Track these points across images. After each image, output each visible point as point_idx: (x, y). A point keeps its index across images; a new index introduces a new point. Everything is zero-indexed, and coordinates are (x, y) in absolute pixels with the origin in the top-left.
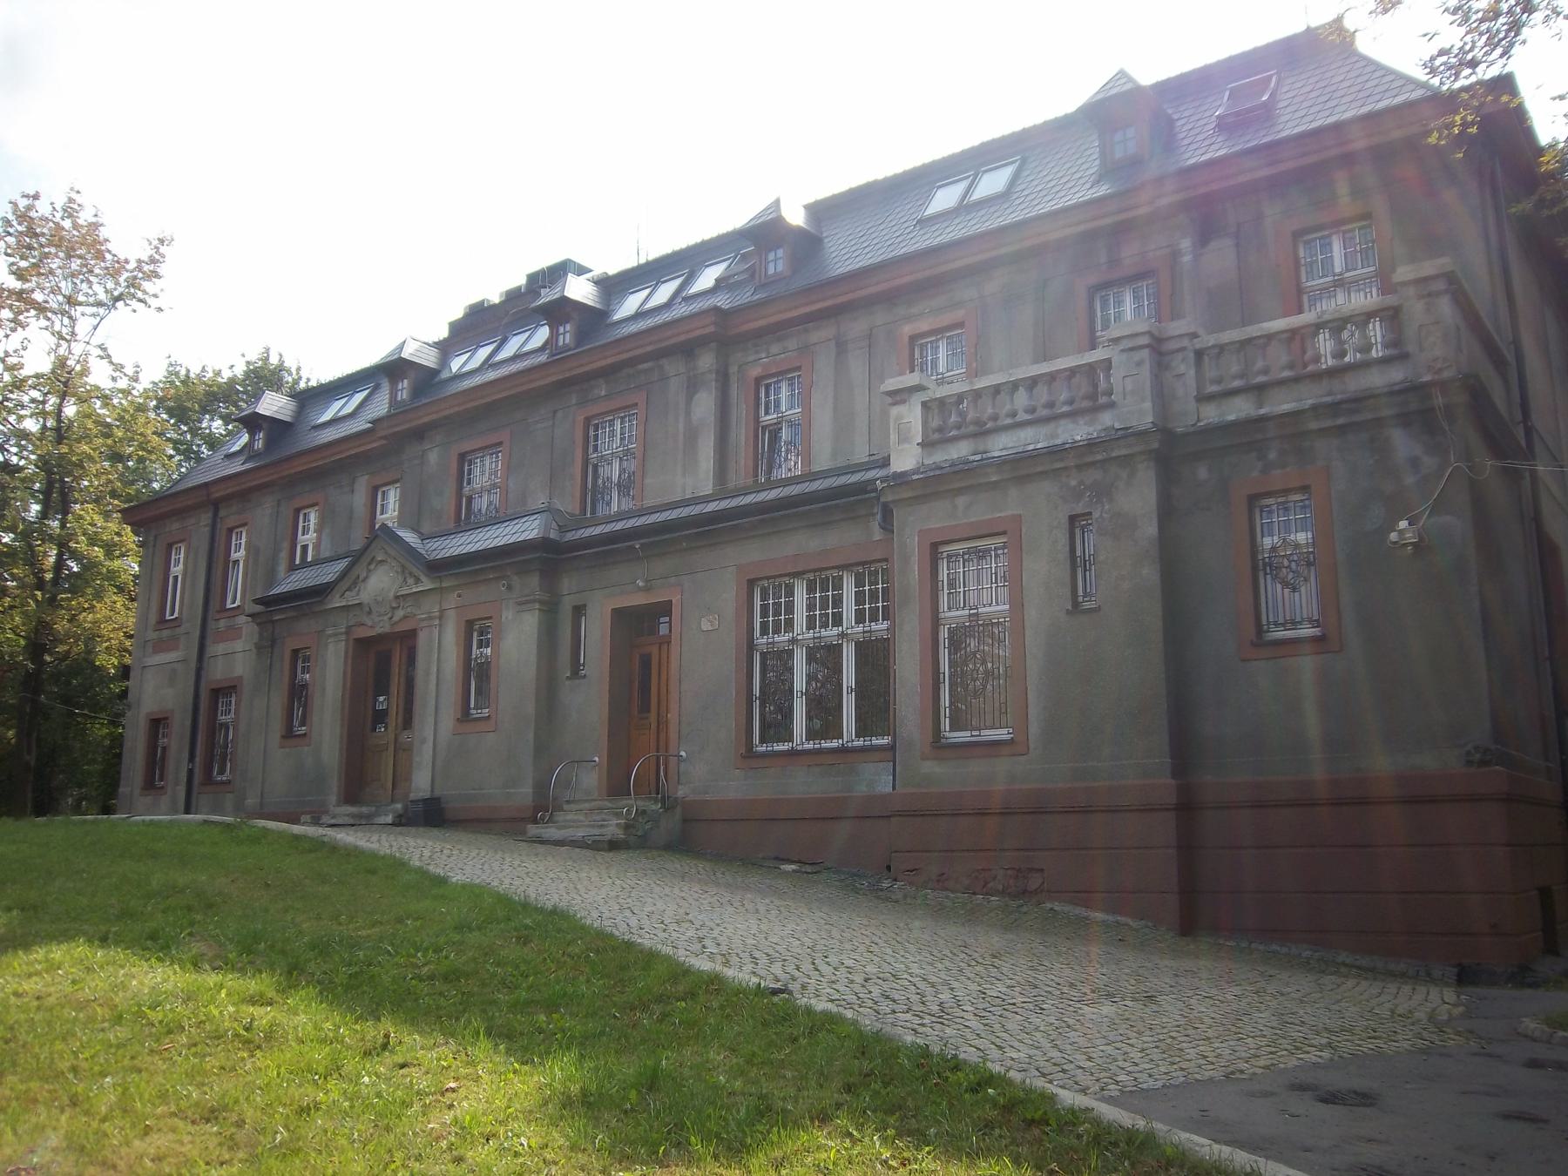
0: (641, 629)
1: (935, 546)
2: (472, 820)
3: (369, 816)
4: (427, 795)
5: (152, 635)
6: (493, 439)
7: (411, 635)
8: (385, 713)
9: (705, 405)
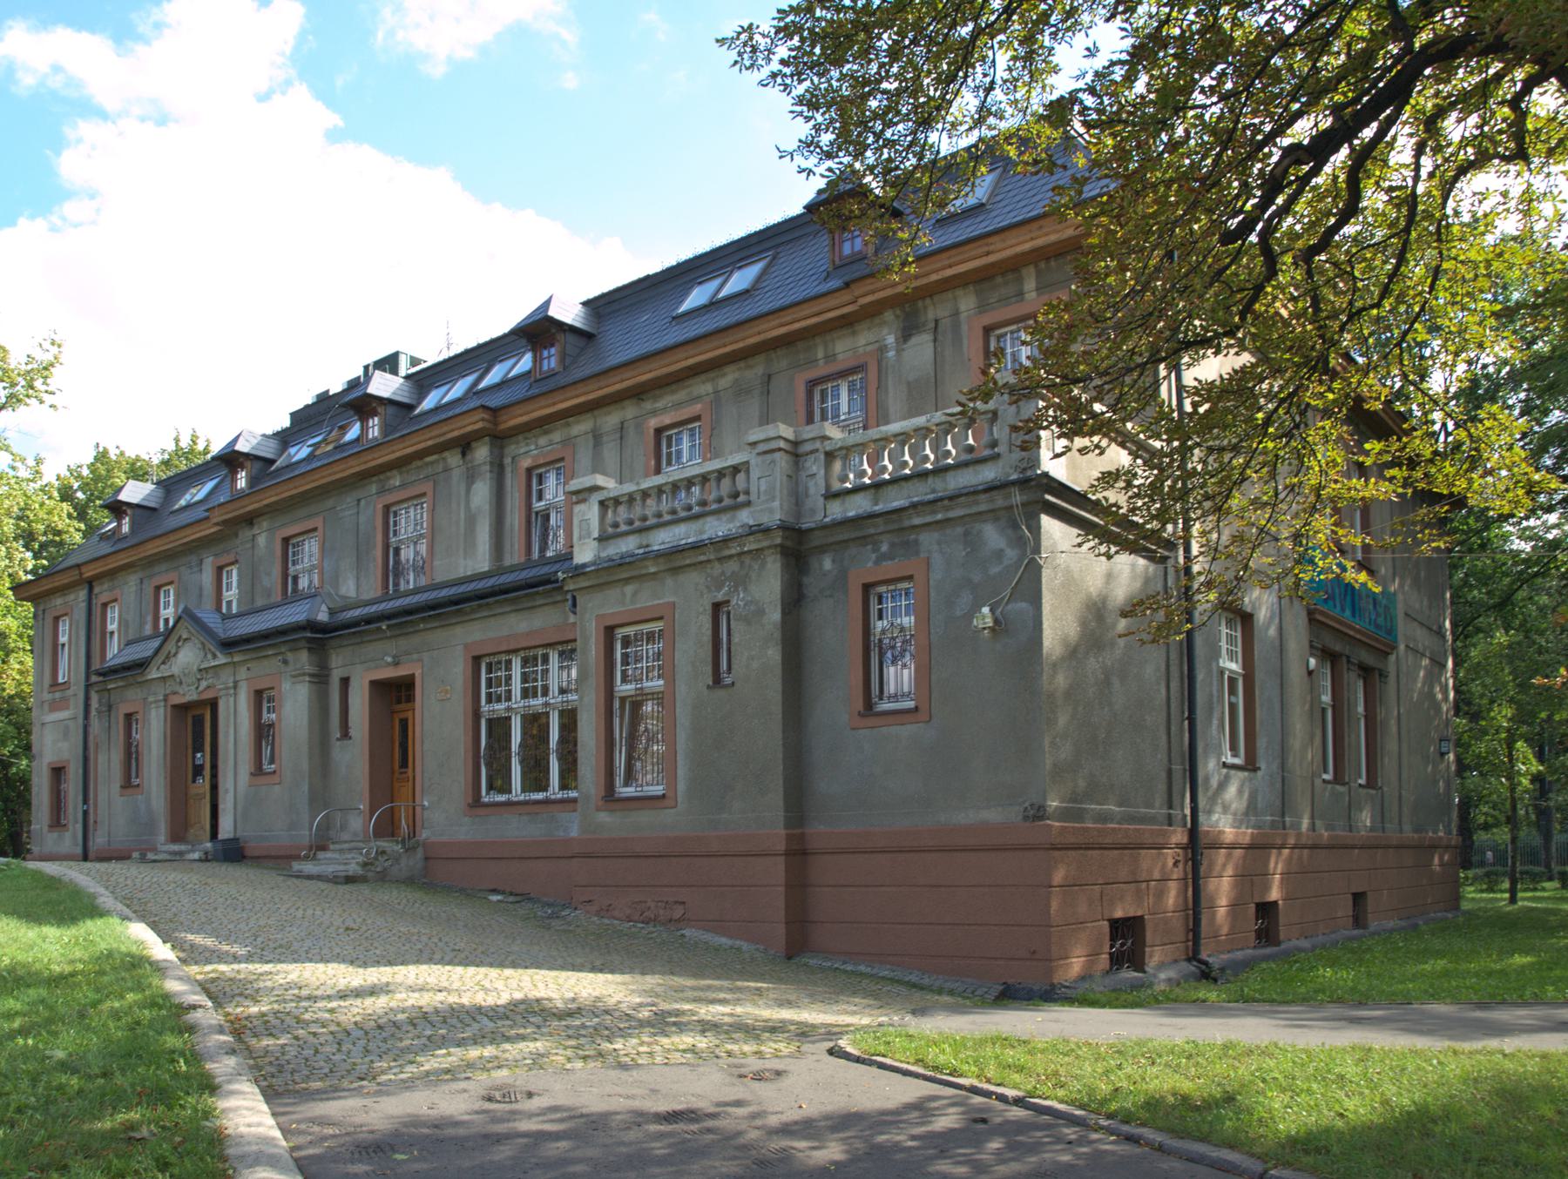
0: (395, 694)
1: (610, 631)
2: (265, 857)
3: (181, 853)
4: (231, 836)
5: (47, 696)
6: (309, 525)
7: (213, 704)
8: (201, 767)
9: (482, 492)
